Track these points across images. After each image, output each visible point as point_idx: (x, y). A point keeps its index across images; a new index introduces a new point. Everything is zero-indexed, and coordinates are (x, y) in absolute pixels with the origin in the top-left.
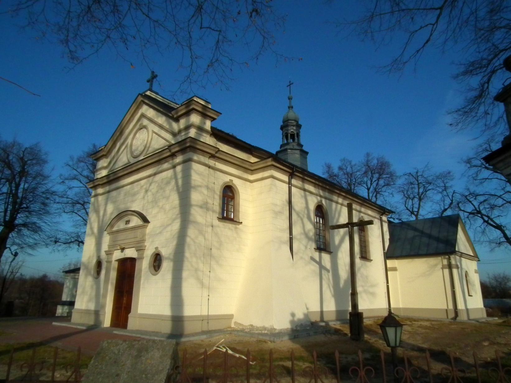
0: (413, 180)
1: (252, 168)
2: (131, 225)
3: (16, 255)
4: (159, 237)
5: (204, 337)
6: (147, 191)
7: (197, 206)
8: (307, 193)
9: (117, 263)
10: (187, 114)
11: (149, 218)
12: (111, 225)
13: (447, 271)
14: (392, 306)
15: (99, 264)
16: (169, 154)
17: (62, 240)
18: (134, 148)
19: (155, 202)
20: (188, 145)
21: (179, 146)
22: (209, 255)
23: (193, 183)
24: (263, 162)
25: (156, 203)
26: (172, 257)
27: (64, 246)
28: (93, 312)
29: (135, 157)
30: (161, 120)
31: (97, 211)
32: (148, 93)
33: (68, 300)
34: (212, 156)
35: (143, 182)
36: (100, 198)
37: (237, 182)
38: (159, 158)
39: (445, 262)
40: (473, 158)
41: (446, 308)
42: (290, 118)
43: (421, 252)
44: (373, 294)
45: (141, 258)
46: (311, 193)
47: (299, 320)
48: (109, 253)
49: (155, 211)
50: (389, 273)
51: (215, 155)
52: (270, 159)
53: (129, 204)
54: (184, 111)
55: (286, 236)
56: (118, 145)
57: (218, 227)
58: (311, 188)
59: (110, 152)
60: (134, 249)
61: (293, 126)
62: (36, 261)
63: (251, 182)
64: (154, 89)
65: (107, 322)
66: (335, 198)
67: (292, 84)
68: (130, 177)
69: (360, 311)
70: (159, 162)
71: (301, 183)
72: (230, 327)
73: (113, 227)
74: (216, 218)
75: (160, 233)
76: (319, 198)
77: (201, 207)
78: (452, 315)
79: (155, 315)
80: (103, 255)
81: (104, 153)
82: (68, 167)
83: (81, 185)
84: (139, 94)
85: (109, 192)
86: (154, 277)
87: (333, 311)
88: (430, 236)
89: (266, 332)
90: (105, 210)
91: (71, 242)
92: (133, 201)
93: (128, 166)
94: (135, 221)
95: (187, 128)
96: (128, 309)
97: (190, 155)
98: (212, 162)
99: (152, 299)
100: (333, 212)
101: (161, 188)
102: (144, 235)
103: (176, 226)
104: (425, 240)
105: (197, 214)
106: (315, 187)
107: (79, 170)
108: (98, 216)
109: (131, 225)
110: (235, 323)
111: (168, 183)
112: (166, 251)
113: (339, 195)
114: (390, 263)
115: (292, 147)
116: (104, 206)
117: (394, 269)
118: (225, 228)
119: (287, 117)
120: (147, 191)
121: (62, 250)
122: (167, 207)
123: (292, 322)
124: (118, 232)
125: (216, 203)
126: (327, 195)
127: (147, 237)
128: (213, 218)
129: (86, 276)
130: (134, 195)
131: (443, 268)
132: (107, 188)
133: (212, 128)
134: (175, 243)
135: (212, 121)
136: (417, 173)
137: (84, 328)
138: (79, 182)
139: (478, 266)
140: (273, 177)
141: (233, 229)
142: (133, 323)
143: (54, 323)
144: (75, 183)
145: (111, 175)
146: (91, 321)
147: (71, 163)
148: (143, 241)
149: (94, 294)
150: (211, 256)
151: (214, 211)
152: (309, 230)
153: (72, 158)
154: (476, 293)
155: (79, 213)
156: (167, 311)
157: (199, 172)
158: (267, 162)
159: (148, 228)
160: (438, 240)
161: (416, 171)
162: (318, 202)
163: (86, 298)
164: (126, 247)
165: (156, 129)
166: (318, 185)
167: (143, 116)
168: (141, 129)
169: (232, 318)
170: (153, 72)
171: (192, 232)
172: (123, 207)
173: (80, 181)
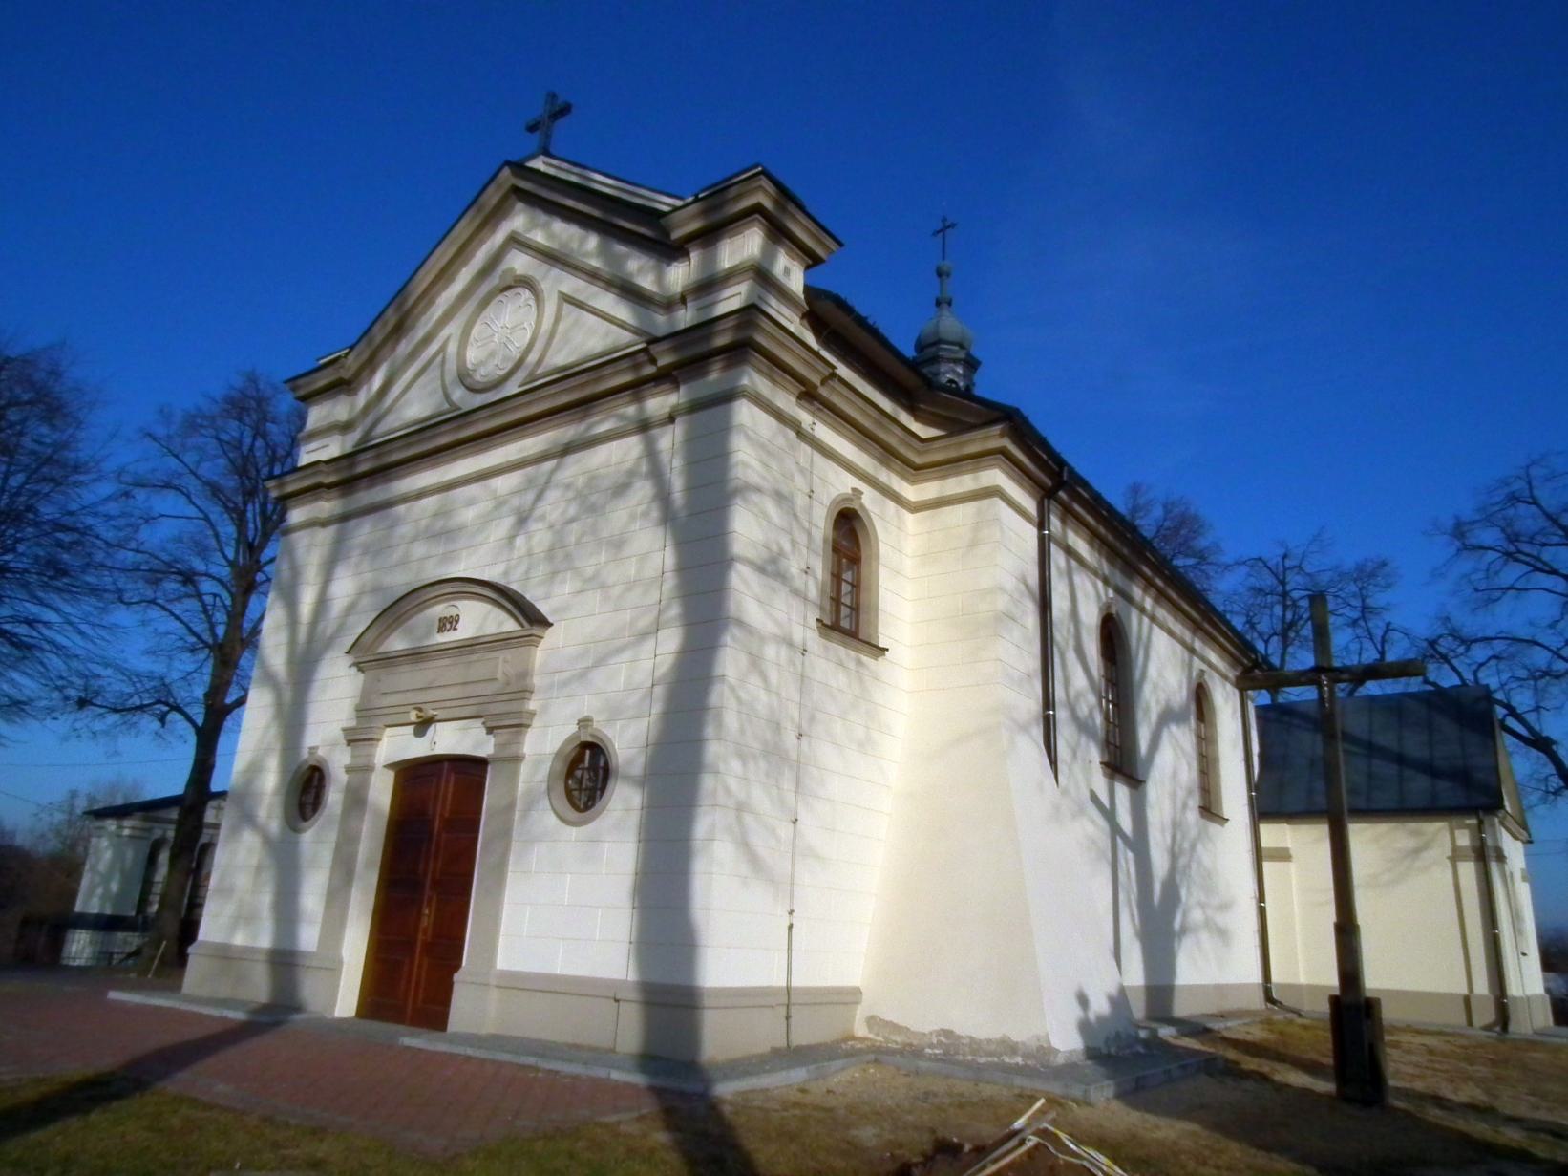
0: (1269, 581)
1: (918, 460)
2: (464, 632)
5: (798, 1075)
7: (750, 563)
9: (391, 775)
10: (710, 235)
11: (544, 608)
13: (1468, 870)
14: (1275, 978)
17: (110, 698)
21: (675, 349)
22: (784, 758)
24: (955, 440)
27: (115, 717)
28: (262, 957)
29: (474, 390)
32: (539, 164)
33: (108, 912)
34: (809, 396)
35: (503, 484)
37: (870, 501)
38: (574, 396)
39: (1464, 839)
40: (1474, 522)
41: (1465, 991)
42: (944, 336)
44: (1222, 934)
47: (1101, 1019)
49: (566, 587)
50: (1267, 866)
52: (997, 429)
54: (695, 226)
55: (1033, 704)
60: (479, 723)
61: (956, 361)
64: (552, 150)
67: (952, 226)
68: (487, 449)
69: (1368, 995)
70: (584, 406)
72: (854, 1038)
74: (814, 624)
77: (761, 570)
78: (1485, 1015)
81: (346, 375)
82: (148, 441)
83: (192, 511)
84: (508, 163)
85: (344, 518)
86: (573, 832)
89: (1019, 1060)
91: (141, 708)
93: (426, 428)
94: (477, 618)
95: (708, 286)
96: (446, 950)
99: (552, 920)
101: (591, 502)
103: (670, 642)
105: (748, 595)
107: (190, 458)
110: (872, 1021)
111: (621, 489)
112: (628, 743)
114: (1274, 834)
117: (1283, 855)
118: (829, 661)
119: (936, 332)
120: (522, 520)
121: (106, 733)
123: (1084, 1027)
125: (810, 566)
128: (801, 622)
133: (807, 289)
135: (808, 268)
136: (1285, 557)
137: (238, 1015)
138: (183, 499)
141: (852, 665)
142: (474, 1008)
143: (114, 995)
144: (168, 503)
145: (362, 456)
146: (259, 988)
147: (161, 431)
152: (1079, 695)
153: (165, 414)
155: (177, 608)
158: (986, 438)
159: (543, 644)
160: (1430, 770)
161: (1282, 551)
164: (440, 714)
165: (571, 284)
166: (1103, 542)
168: (508, 288)
169: (857, 1003)
171: (730, 662)
172: (401, 580)
173: (188, 496)
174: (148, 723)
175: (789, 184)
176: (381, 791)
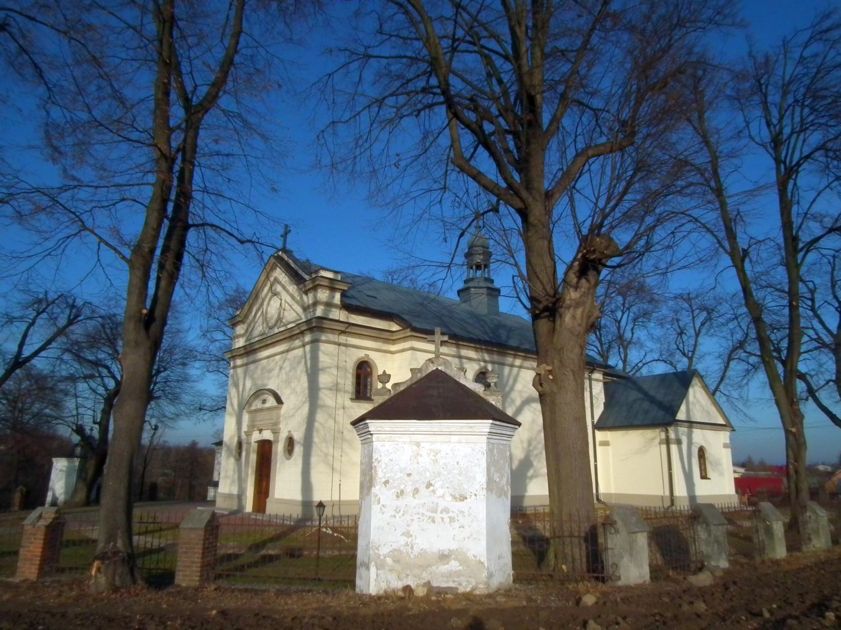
1: (415, 324)
2: (267, 405)
3: (156, 428)
4: (292, 422)
6: (281, 368)
8: (464, 361)
11: (283, 400)
12: (249, 403)
13: (664, 447)
15: (240, 444)
16: (298, 331)
18: (269, 316)
19: (288, 382)
20: (314, 325)
23: (321, 365)
25: (289, 383)
26: (302, 441)
27: (209, 414)
30: (292, 288)
31: (236, 385)
35: (277, 357)
36: (240, 371)
37: (375, 357)
39: (663, 436)
43: (636, 422)
45: (277, 441)
46: (470, 359)
48: (249, 434)
51: (347, 329)
53: (266, 382)
54: (311, 286)
56: (255, 309)
57: (351, 408)
58: (472, 354)
59: (246, 316)
62: (182, 431)
63: (392, 353)
65: (249, 507)
66: (509, 360)
70: (291, 338)
71: (455, 349)
73: (250, 405)
75: (293, 415)
76: (482, 364)
77: (331, 389)
78: (667, 503)
79: (290, 500)
80: (244, 436)
87: (684, 497)
88: (652, 400)
90: (244, 385)
92: (269, 379)
94: (271, 402)
95: (316, 303)
97: (317, 334)
98: (343, 339)
99: (286, 486)
100: (505, 379)
102: (279, 417)
103: (306, 409)
104: (646, 405)
105: (326, 398)
106: (477, 351)
108: (238, 392)
109: (267, 405)
112: (298, 436)
113: (515, 356)
115: (476, 285)
116: (242, 381)
122: (299, 390)
124: (256, 411)
125: (349, 382)
126: (496, 358)
127: (281, 419)
129: (228, 457)
130: (270, 371)
131: (660, 444)
132: (245, 360)
134: (304, 427)
137: (227, 513)
139: (731, 439)
140: (413, 349)
142: (271, 508)
148: (276, 424)
149: (236, 476)
150: (343, 439)
151: (345, 392)
154: (721, 474)
156: (298, 497)
157: (328, 352)
162: (481, 369)
163: (229, 482)
167: (276, 280)
170: (286, 226)
171: (320, 417)
174: (466, 251)
175: (336, 269)
176: (254, 446)
